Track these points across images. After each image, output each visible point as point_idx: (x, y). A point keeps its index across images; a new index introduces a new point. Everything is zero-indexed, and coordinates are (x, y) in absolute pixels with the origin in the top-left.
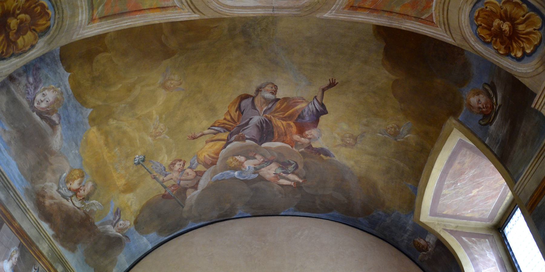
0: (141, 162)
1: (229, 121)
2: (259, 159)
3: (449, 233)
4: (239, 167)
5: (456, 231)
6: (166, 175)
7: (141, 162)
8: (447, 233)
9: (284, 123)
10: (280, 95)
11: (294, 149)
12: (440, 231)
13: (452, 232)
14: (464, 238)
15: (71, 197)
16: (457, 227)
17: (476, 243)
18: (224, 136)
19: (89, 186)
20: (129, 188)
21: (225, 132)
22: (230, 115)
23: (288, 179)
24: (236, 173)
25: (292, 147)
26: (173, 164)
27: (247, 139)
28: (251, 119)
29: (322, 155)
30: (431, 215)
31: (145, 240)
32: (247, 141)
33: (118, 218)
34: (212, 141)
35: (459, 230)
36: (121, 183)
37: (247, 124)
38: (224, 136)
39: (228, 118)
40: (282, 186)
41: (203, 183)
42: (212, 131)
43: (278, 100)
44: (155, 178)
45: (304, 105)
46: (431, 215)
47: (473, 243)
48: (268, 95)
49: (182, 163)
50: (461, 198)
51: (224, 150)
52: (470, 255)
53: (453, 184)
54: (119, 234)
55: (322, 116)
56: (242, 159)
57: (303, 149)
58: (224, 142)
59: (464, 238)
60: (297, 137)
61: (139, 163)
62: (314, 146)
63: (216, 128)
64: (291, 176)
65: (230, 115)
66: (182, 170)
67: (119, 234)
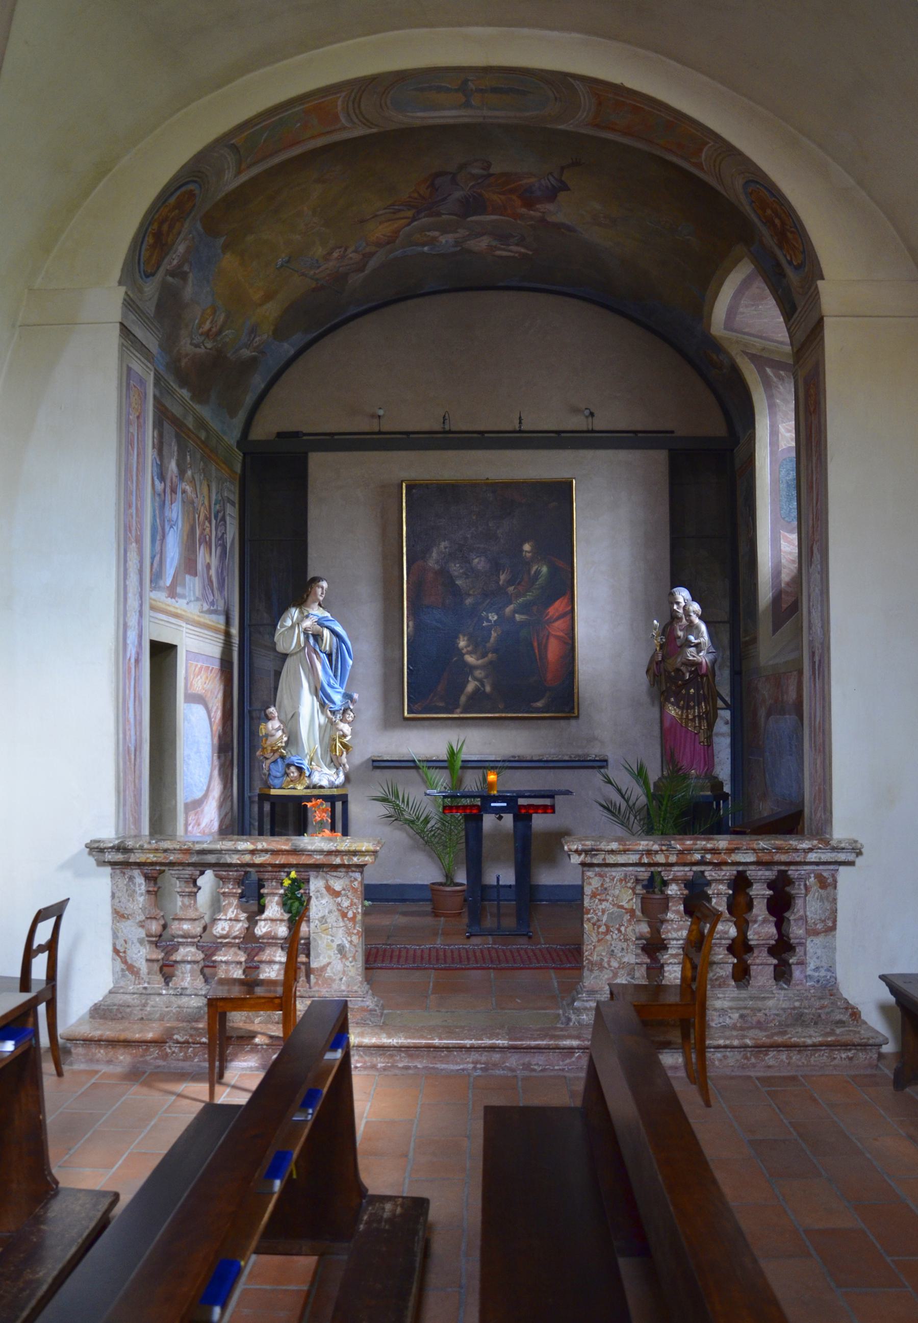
0: (285, 264)
1: (416, 199)
2: (462, 232)
3: (749, 359)
4: (432, 241)
5: (761, 357)
6: (319, 267)
7: (285, 264)
8: (747, 359)
9: (503, 197)
10: (495, 169)
11: (519, 222)
12: (737, 354)
13: (754, 358)
14: (768, 370)
15: (203, 343)
16: (764, 349)
17: (783, 380)
18: (410, 214)
19: (222, 318)
20: (269, 297)
21: (409, 210)
22: (418, 192)
23: (510, 251)
24: (426, 249)
25: (515, 219)
26: (330, 253)
27: (443, 214)
28: (450, 195)
29: (563, 230)
30: (725, 329)
31: (286, 345)
32: (444, 216)
33: (253, 336)
34: (389, 220)
35: (766, 355)
36: (257, 296)
37: (445, 198)
38: (410, 214)
39: (416, 195)
40: (501, 257)
41: (373, 264)
42: (391, 210)
43: (491, 175)
44: (303, 274)
45: (532, 180)
46: (725, 329)
47: (780, 379)
48: (476, 171)
49: (342, 250)
50: (765, 320)
51: (407, 229)
52: (770, 397)
53: (753, 305)
54: (253, 353)
55: (561, 192)
56: (436, 234)
57: (533, 222)
58: (409, 220)
59: (768, 370)
60: (523, 210)
61: (282, 266)
62: (549, 219)
63: (397, 207)
64: (513, 248)
65: (418, 192)
66: (342, 257)
67: (253, 353)
